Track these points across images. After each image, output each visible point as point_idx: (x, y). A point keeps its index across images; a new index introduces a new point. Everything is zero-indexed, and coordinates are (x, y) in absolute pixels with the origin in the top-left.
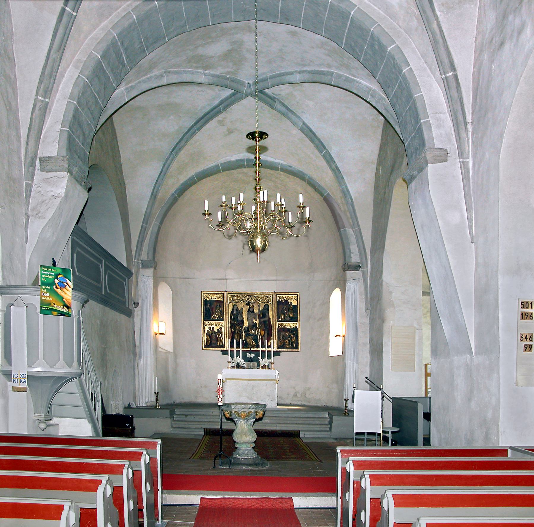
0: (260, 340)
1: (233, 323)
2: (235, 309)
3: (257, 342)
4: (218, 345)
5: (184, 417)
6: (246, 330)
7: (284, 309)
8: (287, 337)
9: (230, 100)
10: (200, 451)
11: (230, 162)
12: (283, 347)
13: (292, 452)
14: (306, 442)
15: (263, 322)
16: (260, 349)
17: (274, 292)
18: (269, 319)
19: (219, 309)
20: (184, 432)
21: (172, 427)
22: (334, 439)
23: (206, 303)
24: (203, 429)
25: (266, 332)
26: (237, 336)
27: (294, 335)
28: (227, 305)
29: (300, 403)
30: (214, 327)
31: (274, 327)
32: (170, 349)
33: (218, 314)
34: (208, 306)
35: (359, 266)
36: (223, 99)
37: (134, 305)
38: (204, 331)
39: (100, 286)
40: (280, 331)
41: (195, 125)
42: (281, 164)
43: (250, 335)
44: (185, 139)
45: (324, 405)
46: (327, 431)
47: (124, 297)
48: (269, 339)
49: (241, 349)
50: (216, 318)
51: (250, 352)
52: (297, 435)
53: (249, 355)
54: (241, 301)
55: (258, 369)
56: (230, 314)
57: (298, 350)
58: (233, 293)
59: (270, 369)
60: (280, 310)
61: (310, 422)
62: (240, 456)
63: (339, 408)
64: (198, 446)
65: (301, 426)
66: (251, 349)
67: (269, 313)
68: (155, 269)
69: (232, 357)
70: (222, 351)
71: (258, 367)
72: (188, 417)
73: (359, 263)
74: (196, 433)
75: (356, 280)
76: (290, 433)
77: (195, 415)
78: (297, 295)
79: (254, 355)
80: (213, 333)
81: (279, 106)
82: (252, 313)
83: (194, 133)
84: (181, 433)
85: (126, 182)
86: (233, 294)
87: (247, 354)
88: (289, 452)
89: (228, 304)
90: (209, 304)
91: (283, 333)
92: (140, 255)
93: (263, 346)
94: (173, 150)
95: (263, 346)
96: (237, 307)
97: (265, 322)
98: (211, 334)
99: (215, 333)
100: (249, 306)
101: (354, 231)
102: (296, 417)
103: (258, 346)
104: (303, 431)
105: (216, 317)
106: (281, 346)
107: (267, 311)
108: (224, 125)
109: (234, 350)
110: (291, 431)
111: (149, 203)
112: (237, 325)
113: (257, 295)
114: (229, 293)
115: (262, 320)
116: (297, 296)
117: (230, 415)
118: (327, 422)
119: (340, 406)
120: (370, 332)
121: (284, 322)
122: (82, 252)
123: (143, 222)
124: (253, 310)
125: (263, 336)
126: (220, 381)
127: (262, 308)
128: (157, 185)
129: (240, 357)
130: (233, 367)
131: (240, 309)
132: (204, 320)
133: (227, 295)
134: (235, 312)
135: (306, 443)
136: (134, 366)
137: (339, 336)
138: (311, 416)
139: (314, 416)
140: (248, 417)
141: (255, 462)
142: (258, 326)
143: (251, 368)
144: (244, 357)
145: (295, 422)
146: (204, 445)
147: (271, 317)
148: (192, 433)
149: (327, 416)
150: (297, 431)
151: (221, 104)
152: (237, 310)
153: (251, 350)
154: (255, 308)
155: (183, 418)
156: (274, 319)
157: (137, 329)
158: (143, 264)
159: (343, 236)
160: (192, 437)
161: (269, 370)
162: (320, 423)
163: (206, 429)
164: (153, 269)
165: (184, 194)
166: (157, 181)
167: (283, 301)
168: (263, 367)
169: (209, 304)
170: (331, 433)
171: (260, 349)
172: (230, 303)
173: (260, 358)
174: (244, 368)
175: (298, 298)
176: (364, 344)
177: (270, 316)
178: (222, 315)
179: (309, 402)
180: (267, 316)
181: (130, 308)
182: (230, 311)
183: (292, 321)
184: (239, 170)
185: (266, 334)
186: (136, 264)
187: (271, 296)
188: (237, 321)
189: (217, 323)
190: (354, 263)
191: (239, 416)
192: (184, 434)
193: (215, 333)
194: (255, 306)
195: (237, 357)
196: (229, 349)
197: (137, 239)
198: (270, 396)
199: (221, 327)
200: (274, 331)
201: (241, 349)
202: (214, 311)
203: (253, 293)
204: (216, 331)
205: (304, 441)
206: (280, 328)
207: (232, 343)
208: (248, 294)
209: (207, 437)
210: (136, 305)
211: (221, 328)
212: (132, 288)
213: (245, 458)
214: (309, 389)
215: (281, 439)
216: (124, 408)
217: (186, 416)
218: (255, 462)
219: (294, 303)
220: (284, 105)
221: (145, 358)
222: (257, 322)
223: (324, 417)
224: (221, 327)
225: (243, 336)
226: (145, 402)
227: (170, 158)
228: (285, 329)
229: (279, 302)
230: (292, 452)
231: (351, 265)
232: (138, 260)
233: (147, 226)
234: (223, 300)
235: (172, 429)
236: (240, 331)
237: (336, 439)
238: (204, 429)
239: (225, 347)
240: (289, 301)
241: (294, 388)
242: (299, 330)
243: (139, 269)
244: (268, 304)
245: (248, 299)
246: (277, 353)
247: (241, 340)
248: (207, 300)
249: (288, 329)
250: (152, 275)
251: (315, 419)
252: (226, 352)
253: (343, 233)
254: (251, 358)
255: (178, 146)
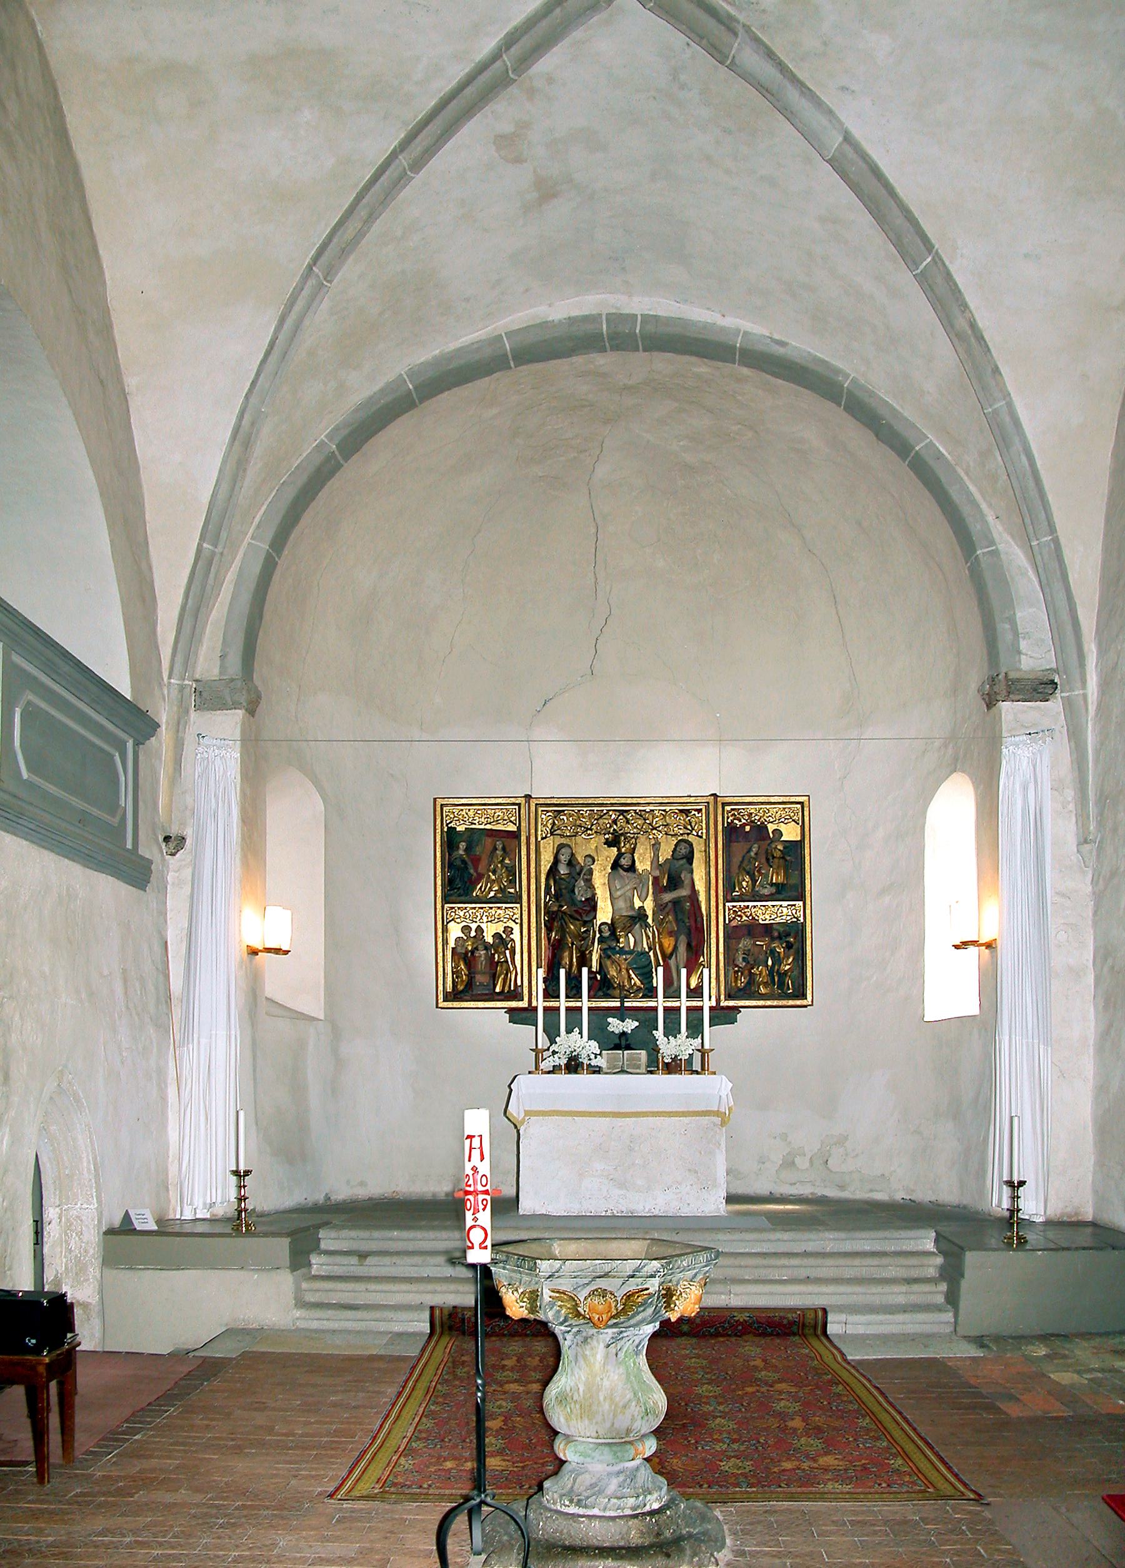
0: (660, 970)
1: (555, 909)
2: (563, 858)
3: (646, 975)
4: (498, 990)
5: (354, 1260)
6: (607, 934)
7: (752, 854)
8: (762, 957)
9: (544, 24)
10: (393, 1443)
11: (545, 325)
12: (748, 992)
13: (818, 1430)
14: (861, 1362)
15: (670, 904)
16: (660, 1003)
17: (715, 795)
18: (694, 893)
19: (502, 861)
20: (349, 1325)
21: (301, 1304)
22: (969, 1339)
23: (451, 839)
24: (426, 1315)
25: (683, 939)
26: (569, 957)
27: (789, 946)
28: (533, 847)
29: (806, 1191)
30: (484, 926)
31: (713, 923)
32: (313, 1005)
33: (499, 881)
34: (461, 852)
35: (1053, 682)
36: (516, 29)
37: (163, 845)
38: (445, 942)
39: (115, 821)
40: (732, 934)
41: (402, 151)
42: (746, 333)
43: (622, 951)
44: (362, 212)
45: (899, 1196)
46: (938, 1309)
47: (113, 807)
48: (692, 965)
49: (585, 1003)
50: (492, 894)
51: (622, 1013)
52: (815, 1327)
53: (616, 1025)
54: (588, 829)
55: (651, 1072)
56: (543, 880)
57: (804, 1002)
58: (554, 801)
59: (697, 1073)
60: (736, 860)
61: (864, 1272)
62: (579, 1504)
63: (965, 1207)
64: (394, 1405)
65: (831, 1289)
66: (622, 1003)
67: (692, 872)
68: (251, 712)
69: (552, 1033)
70: (510, 1011)
71: (656, 1065)
72: (370, 1260)
73: (1056, 671)
74: (397, 1328)
75: (1040, 735)
76: (785, 1322)
77: (397, 1253)
78: (800, 810)
79: (637, 1024)
80: (480, 947)
81: (750, 58)
82: (629, 874)
83: (401, 180)
84: (335, 1325)
85: (131, 382)
86: (558, 808)
87: (610, 1020)
88: (766, 1369)
89: (537, 844)
90: (463, 845)
91: (745, 943)
92: (188, 662)
93: (672, 990)
94: (315, 260)
95: (672, 990)
96: (573, 855)
97: (676, 903)
98: (472, 952)
99: (487, 946)
100: (615, 849)
101: (1036, 549)
102: (806, 1254)
103: (651, 993)
104: (841, 1309)
105: (491, 890)
106: (740, 990)
107: (687, 866)
108: (518, 160)
109: (558, 1009)
110: (792, 1310)
111: (224, 462)
112: (571, 916)
113: (648, 809)
114: (542, 801)
115: (668, 897)
116: (799, 806)
117: (533, 1309)
118: (932, 1272)
119: (966, 1201)
120: (1095, 924)
121: (751, 904)
122: (43, 705)
123: (202, 538)
124: (634, 861)
125: (671, 954)
126: (476, 1142)
127: (666, 853)
128: (253, 400)
129: (581, 1033)
130: (555, 1070)
131: (580, 859)
132: (446, 899)
133: (533, 808)
134: (563, 870)
135: (857, 1365)
136: (161, 1072)
137: (974, 943)
138: (867, 1248)
139: (877, 1247)
140: (622, 1319)
141: (658, 1534)
142: (650, 920)
143: (623, 1072)
144: (599, 1033)
145: (803, 1273)
146: (419, 1393)
147: (700, 886)
148: (383, 1327)
149: (930, 1246)
150: (815, 1310)
151: (508, 48)
152: (571, 863)
153: (626, 1004)
154: (641, 854)
155: (350, 1265)
156: (713, 893)
157: (174, 934)
158: (205, 694)
159: (988, 576)
160: (377, 1348)
161: (695, 1076)
162: (902, 1273)
163: (437, 1312)
164: (240, 713)
165: (366, 447)
166: (254, 383)
167: (748, 828)
168: (673, 1067)
169: (463, 845)
170: (956, 1316)
171: (660, 1003)
172: (543, 839)
173: (659, 1034)
174: (597, 1070)
175: (806, 813)
176: (1075, 973)
177: (697, 883)
178: (512, 882)
179: (842, 1188)
180: (687, 882)
181: (143, 851)
182: (545, 867)
183: (781, 897)
184: (578, 360)
185: (682, 948)
186: (176, 692)
187: (699, 811)
188: (572, 902)
189: (499, 910)
190: (1032, 671)
191: (578, 1315)
192: (349, 1332)
193: (486, 948)
194: (640, 850)
195: (569, 1031)
196: (540, 1003)
197: (179, 600)
198: (696, 1172)
199: (511, 924)
200: (713, 935)
201: (585, 1003)
202: (481, 868)
203: (634, 801)
204: (489, 939)
205: (849, 1358)
206: (734, 923)
207: (551, 981)
208: (612, 805)
209: (446, 1346)
210: (172, 845)
211: (509, 931)
212: (156, 781)
213: (607, 1514)
214: (842, 1140)
215: (751, 1349)
216: (105, 1233)
217: (363, 1256)
218: (658, 1534)
219: (790, 833)
220: (770, 55)
221: (203, 1041)
222: (649, 906)
223: (920, 1248)
224: (511, 924)
225: (595, 957)
226: (205, 1204)
227: (306, 293)
228: (753, 929)
229: (731, 832)
230: (818, 1430)
231: (1018, 680)
232: (184, 680)
233: (219, 550)
234: (519, 828)
235: (298, 1313)
236: (584, 939)
237: (979, 1341)
238: (432, 1308)
239: (526, 998)
240: (771, 828)
241: (784, 1137)
242: (808, 930)
243: (187, 712)
244: (691, 838)
245: (615, 822)
246: (723, 1015)
247: (585, 970)
248: (458, 829)
249: (768, 929)
250: (237, 734)
251: (885, 1261)
252: (528, 1014)
253: (984, 562)
254: (624, 1034)
255: (335, 240)
